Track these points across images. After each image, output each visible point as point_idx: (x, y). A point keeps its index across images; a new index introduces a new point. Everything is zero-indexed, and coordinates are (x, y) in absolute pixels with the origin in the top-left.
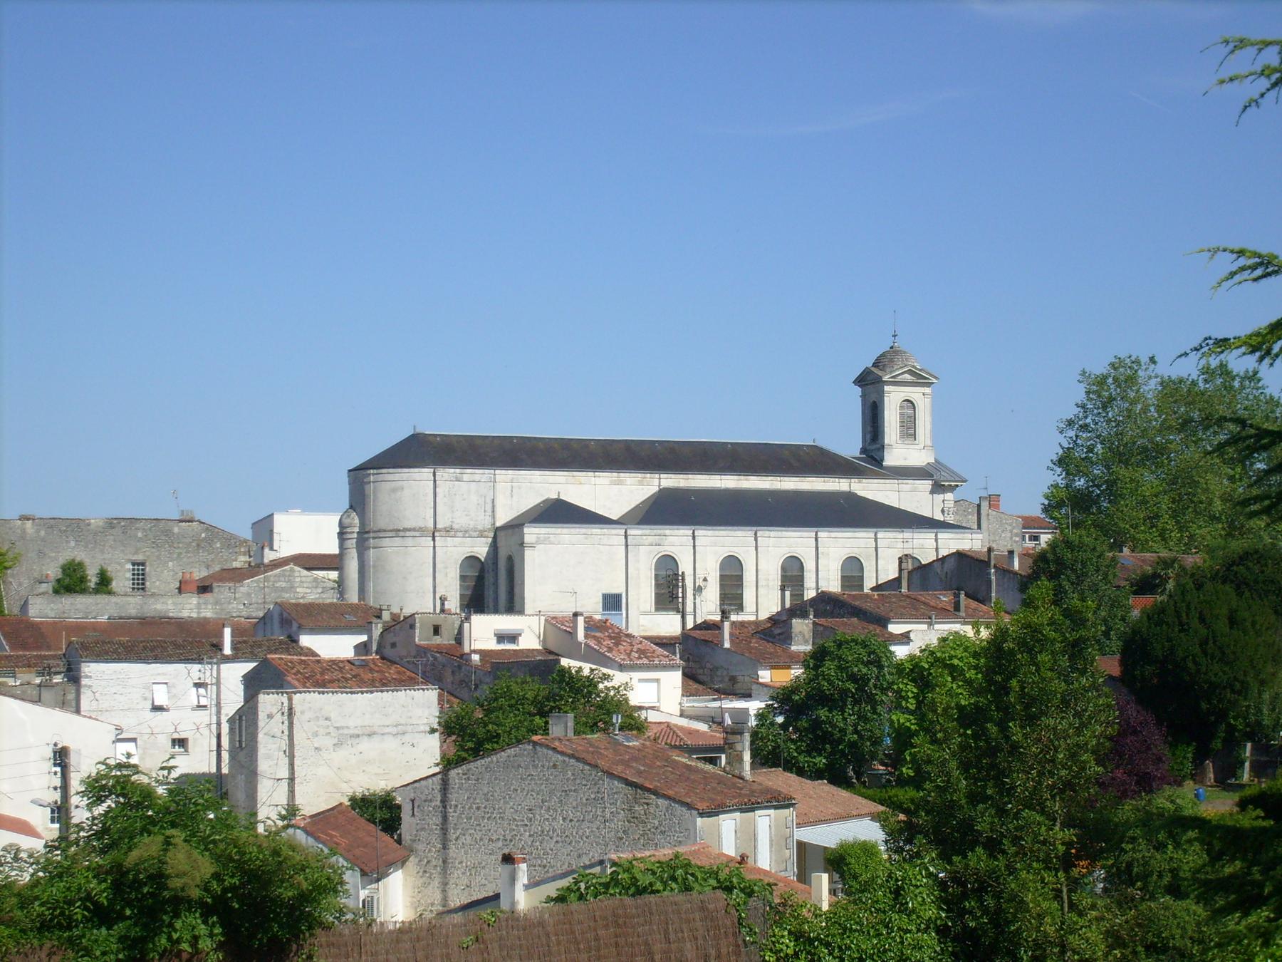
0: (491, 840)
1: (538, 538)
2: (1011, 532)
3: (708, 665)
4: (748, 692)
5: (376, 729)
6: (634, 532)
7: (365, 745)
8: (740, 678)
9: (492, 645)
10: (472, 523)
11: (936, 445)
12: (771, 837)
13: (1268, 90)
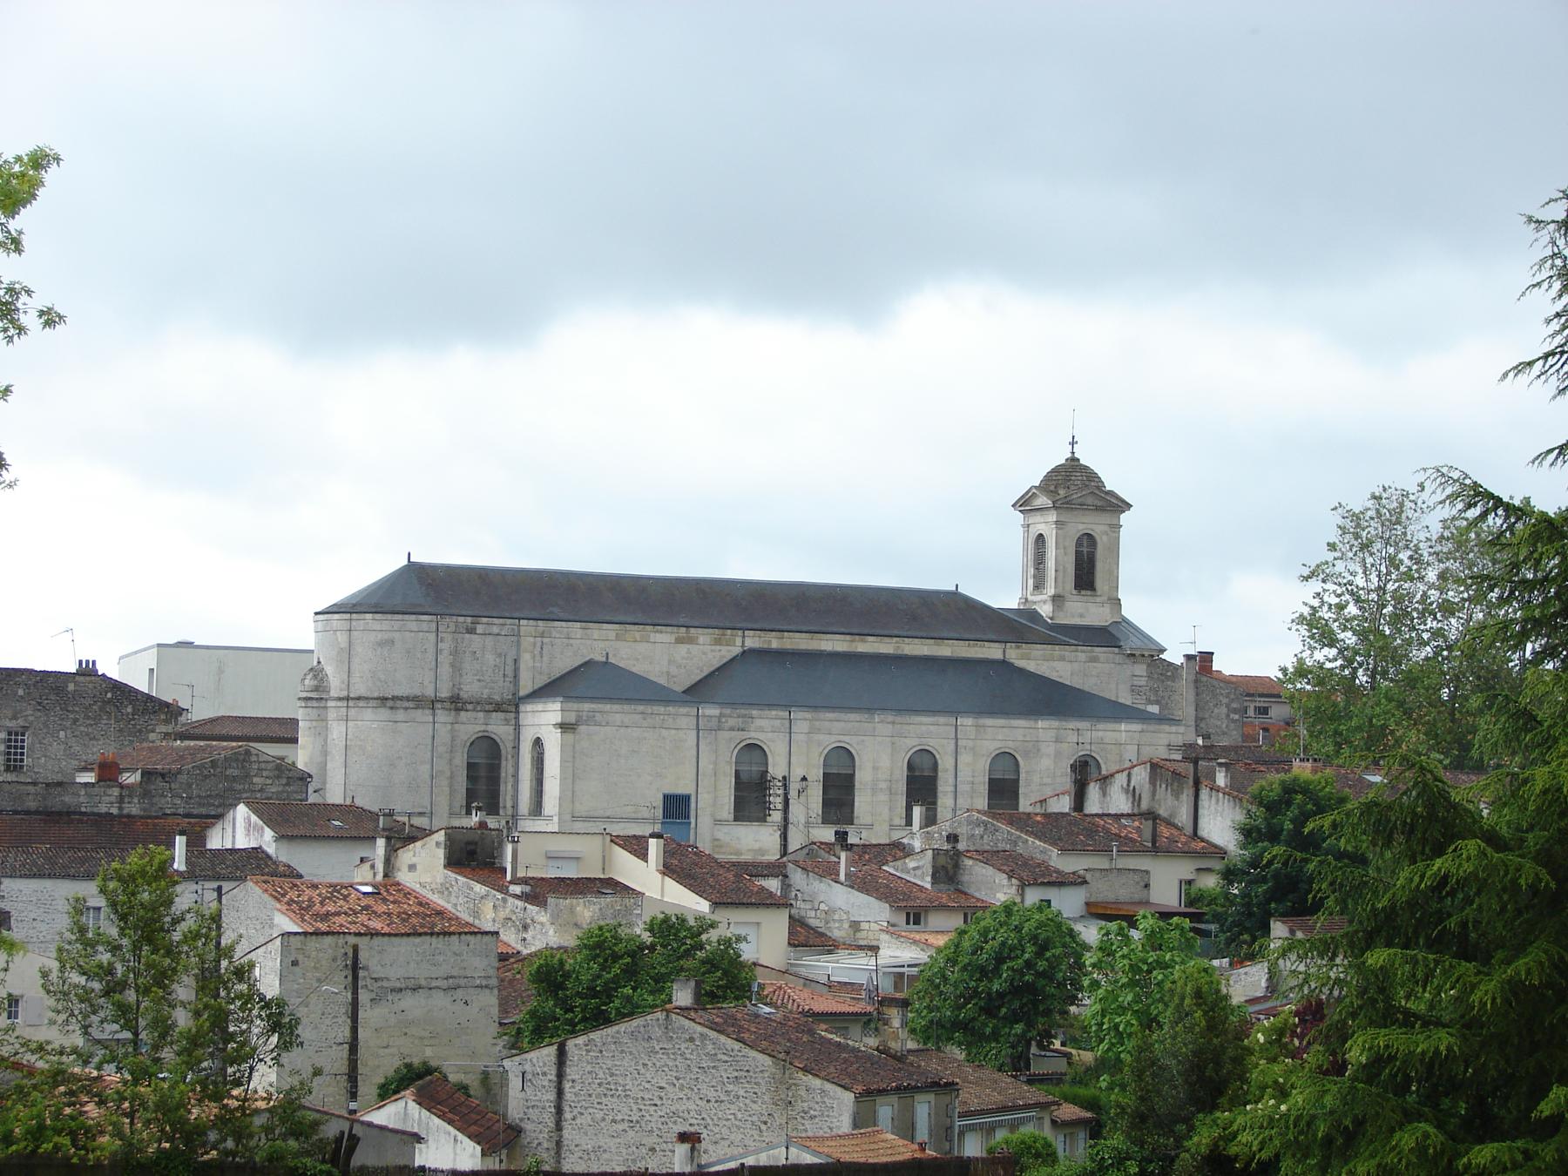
0: (614, 1121)
1: (579, 716)
2: (1228, 706)
3: (823, 906)
4: (874, 943)
5: (423, 983)
7: (408, 1001)
8: (864, 926)
10: (486, 691)
12: (930, 1126)
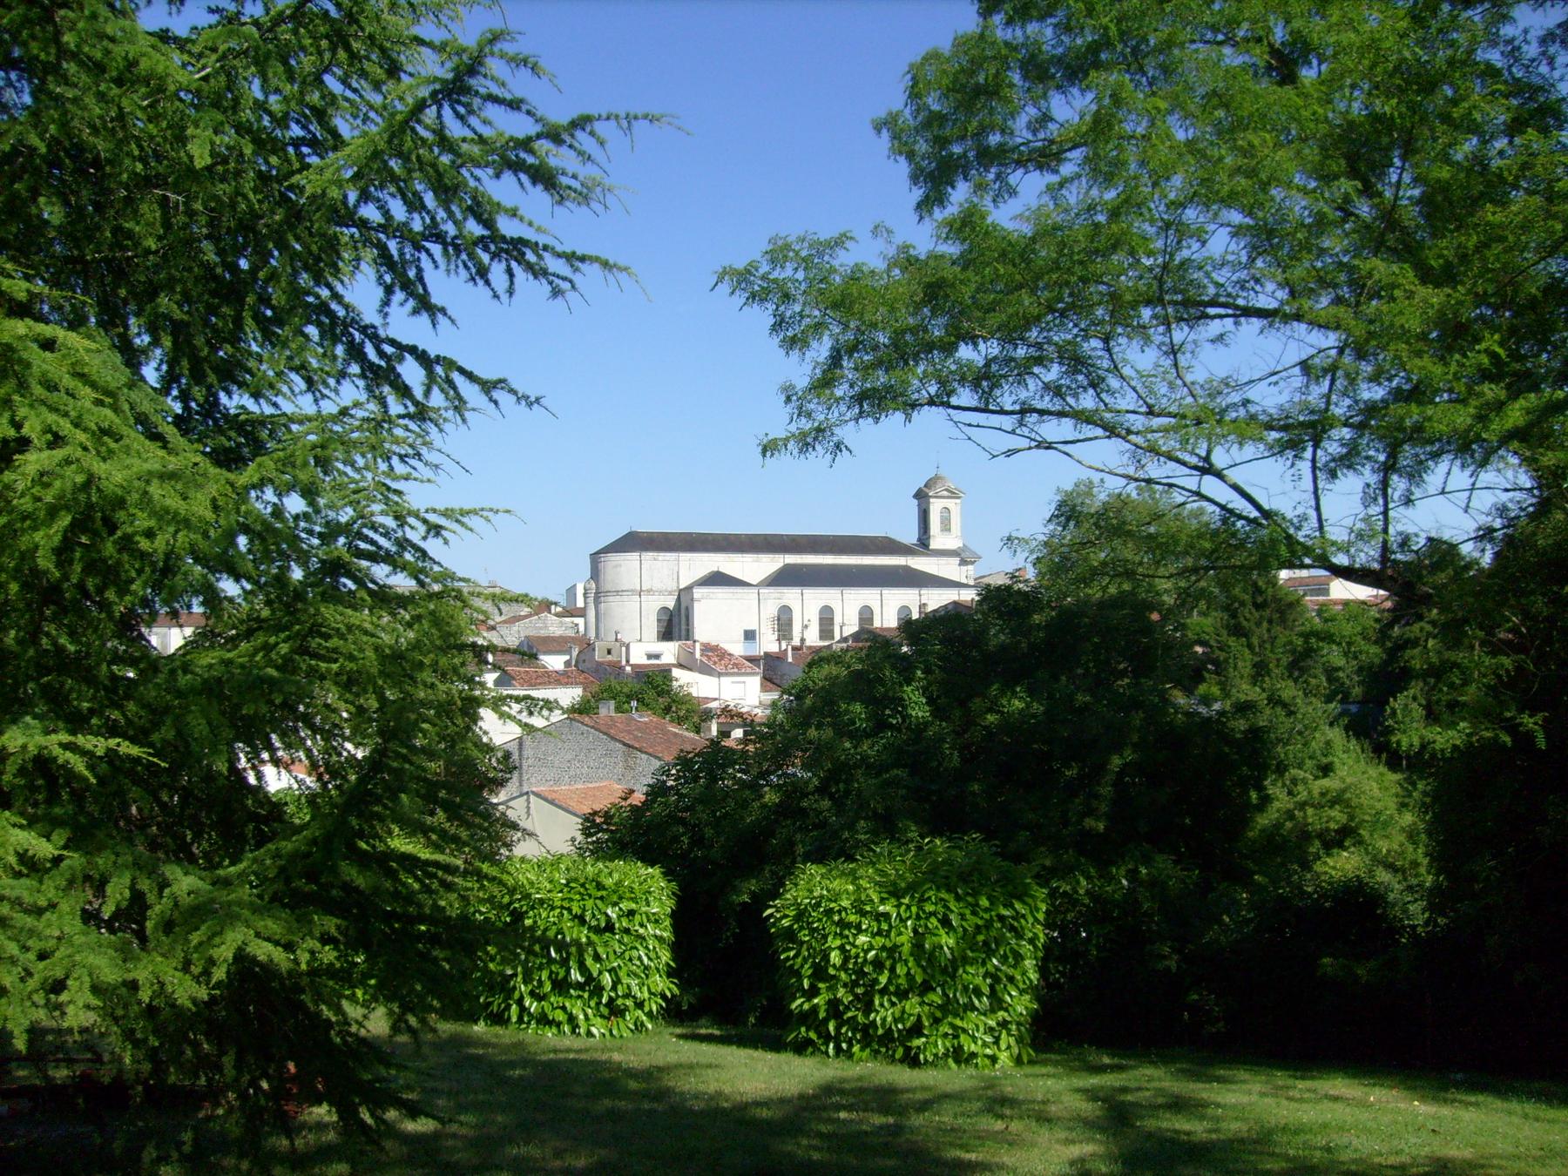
6: (764, 591)
9: (644, 661)
11: (963, 536)
13: (521, 219)
